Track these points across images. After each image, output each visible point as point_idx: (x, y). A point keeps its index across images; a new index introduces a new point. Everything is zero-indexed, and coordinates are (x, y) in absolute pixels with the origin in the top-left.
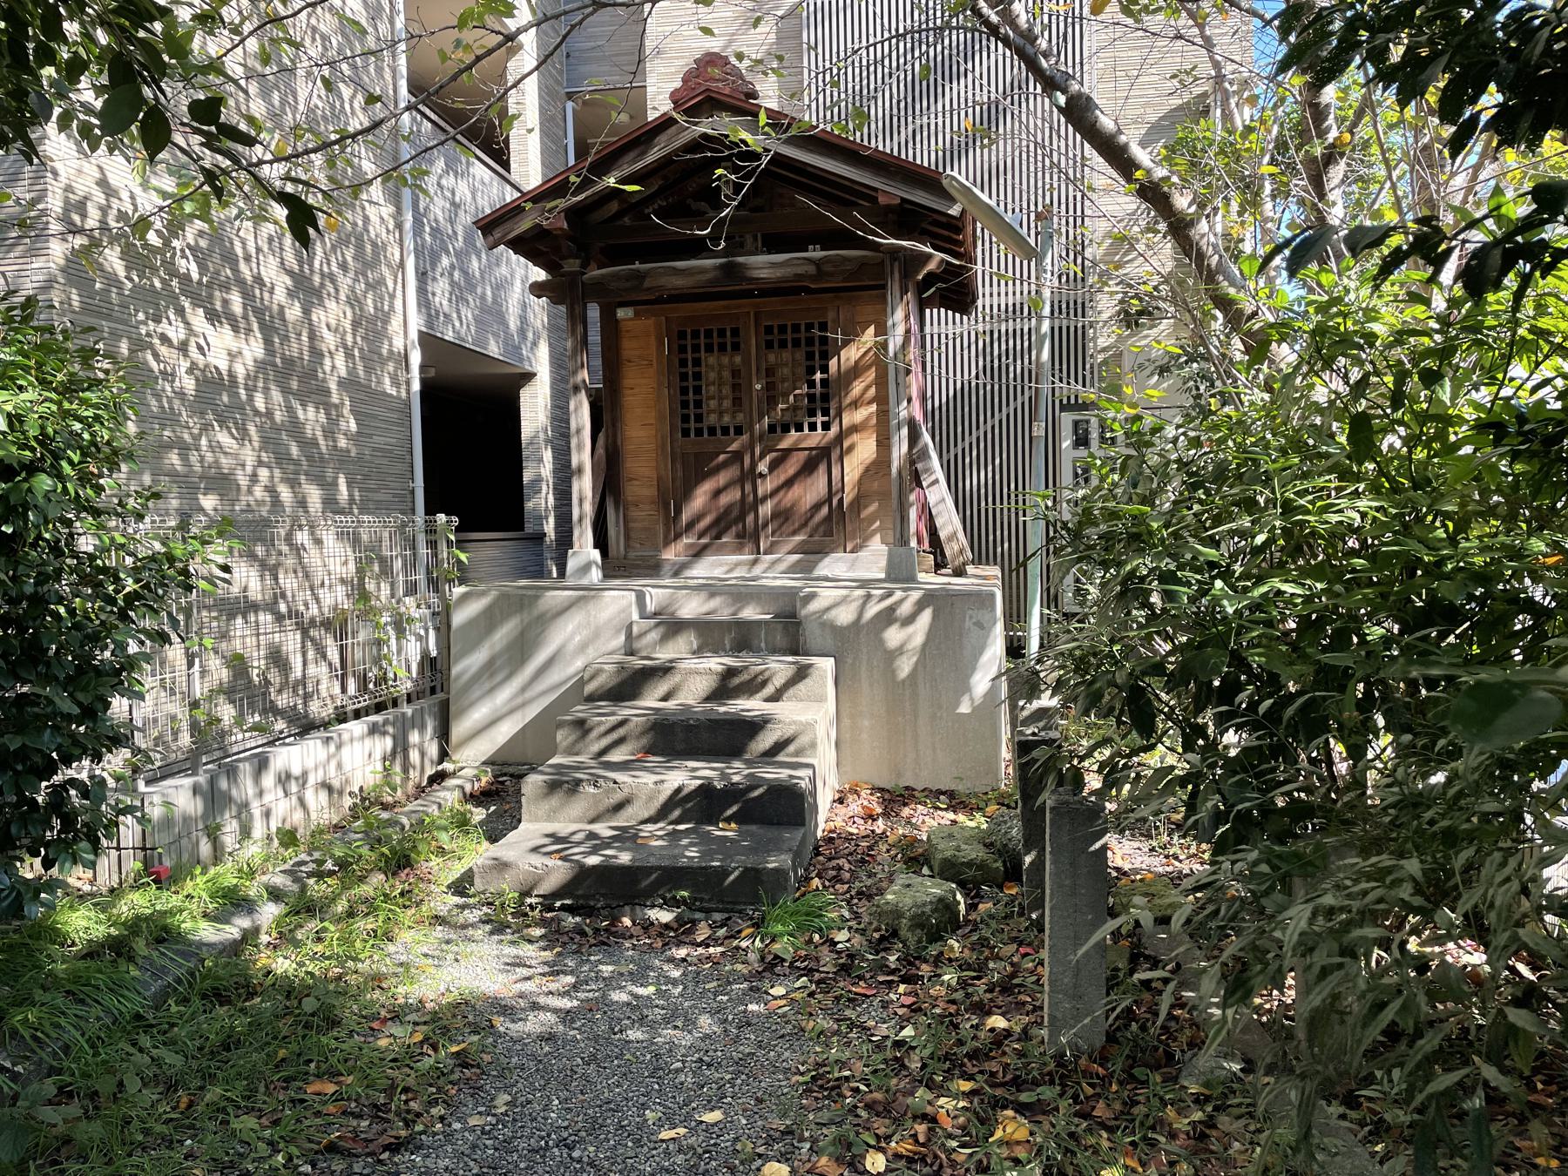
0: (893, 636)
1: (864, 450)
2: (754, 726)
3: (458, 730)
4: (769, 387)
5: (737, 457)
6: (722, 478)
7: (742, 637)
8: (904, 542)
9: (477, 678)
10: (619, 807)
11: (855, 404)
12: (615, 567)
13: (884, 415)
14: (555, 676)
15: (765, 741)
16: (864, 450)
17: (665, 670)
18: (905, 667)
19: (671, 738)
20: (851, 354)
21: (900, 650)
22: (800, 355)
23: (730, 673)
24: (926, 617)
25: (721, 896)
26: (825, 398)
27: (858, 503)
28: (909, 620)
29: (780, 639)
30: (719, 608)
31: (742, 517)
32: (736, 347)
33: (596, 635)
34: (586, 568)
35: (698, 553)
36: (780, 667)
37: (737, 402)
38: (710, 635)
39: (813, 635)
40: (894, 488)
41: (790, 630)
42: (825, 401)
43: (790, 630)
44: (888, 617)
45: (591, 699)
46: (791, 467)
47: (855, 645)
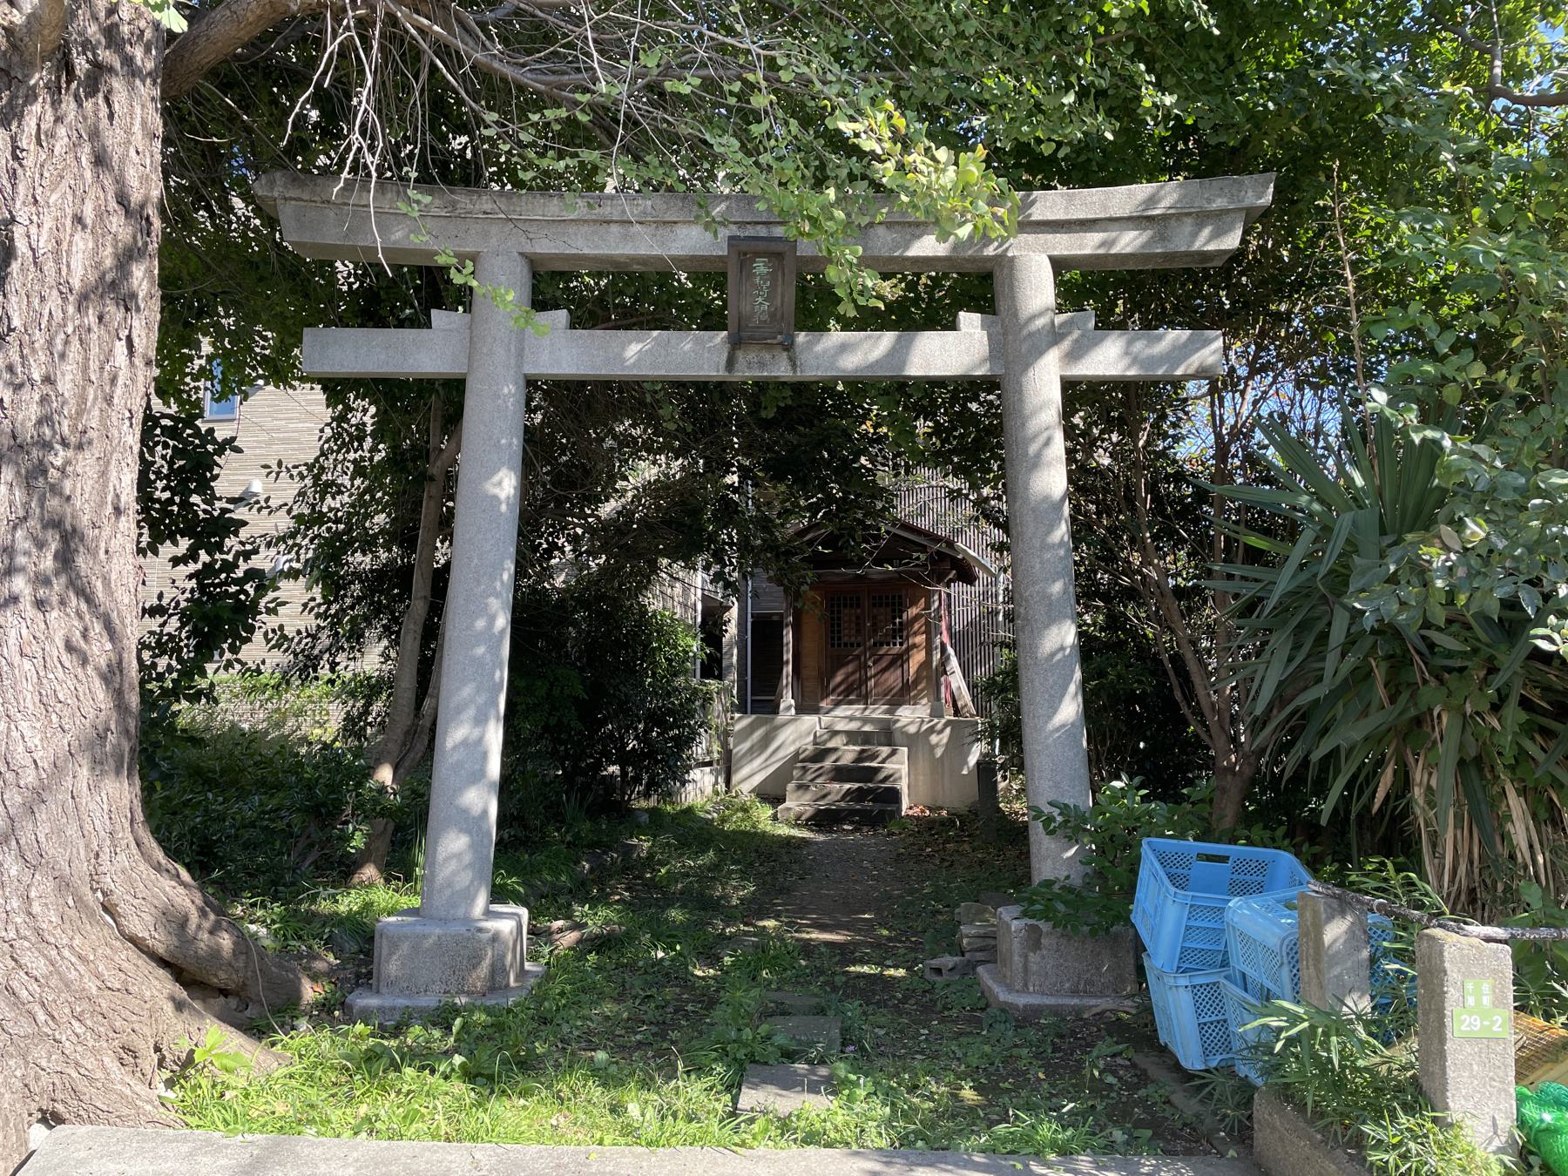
0: (934, 739)
1: (918, 658)
2: (877, 770)
3: (735, 779)
4: (874, 625)
5: (858, 657)
6: (850, 668)
7: (865, 738)
8: (938, 699)
9: (745, 755)
10: (824, 796)
11: (915, 634)
12: (802, 709)
13: (929, 641)
14: (781, 754)
15: (881, 776)
16: (918, 658)
17: (835, 750)
18: (939, 752)
19: (840, 774)
20: (913, 611)
21: (937, 745)
22: (889, 609)
23: (863, 751)
24: (948, 730)
25: (867, 820)
26: (901, 631)
27: (916, 682)
28: (941, 731)
29: (883, 739)
30: (853, 726)
31: (860, 687)
32: (858, 606)
33: (800, 737)
34: (789, 708)
35: (837, 704)
36: (885, 750)
37: (858, 631)
38: (852, 737)
39: (898, 737)
40: (933, 675)
41: (887, 735)
42: (902, 631)
43: (887, 735)
44: (931, 730)
45: (803, 761)
46: (883, 664)
47: (917, 741)
